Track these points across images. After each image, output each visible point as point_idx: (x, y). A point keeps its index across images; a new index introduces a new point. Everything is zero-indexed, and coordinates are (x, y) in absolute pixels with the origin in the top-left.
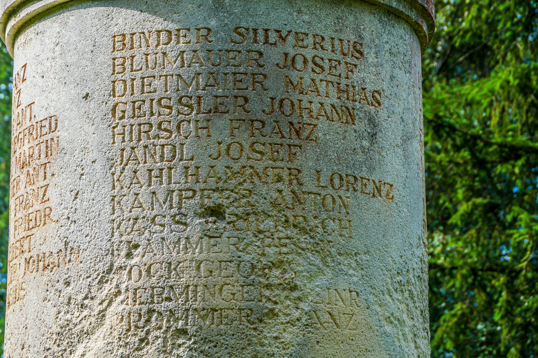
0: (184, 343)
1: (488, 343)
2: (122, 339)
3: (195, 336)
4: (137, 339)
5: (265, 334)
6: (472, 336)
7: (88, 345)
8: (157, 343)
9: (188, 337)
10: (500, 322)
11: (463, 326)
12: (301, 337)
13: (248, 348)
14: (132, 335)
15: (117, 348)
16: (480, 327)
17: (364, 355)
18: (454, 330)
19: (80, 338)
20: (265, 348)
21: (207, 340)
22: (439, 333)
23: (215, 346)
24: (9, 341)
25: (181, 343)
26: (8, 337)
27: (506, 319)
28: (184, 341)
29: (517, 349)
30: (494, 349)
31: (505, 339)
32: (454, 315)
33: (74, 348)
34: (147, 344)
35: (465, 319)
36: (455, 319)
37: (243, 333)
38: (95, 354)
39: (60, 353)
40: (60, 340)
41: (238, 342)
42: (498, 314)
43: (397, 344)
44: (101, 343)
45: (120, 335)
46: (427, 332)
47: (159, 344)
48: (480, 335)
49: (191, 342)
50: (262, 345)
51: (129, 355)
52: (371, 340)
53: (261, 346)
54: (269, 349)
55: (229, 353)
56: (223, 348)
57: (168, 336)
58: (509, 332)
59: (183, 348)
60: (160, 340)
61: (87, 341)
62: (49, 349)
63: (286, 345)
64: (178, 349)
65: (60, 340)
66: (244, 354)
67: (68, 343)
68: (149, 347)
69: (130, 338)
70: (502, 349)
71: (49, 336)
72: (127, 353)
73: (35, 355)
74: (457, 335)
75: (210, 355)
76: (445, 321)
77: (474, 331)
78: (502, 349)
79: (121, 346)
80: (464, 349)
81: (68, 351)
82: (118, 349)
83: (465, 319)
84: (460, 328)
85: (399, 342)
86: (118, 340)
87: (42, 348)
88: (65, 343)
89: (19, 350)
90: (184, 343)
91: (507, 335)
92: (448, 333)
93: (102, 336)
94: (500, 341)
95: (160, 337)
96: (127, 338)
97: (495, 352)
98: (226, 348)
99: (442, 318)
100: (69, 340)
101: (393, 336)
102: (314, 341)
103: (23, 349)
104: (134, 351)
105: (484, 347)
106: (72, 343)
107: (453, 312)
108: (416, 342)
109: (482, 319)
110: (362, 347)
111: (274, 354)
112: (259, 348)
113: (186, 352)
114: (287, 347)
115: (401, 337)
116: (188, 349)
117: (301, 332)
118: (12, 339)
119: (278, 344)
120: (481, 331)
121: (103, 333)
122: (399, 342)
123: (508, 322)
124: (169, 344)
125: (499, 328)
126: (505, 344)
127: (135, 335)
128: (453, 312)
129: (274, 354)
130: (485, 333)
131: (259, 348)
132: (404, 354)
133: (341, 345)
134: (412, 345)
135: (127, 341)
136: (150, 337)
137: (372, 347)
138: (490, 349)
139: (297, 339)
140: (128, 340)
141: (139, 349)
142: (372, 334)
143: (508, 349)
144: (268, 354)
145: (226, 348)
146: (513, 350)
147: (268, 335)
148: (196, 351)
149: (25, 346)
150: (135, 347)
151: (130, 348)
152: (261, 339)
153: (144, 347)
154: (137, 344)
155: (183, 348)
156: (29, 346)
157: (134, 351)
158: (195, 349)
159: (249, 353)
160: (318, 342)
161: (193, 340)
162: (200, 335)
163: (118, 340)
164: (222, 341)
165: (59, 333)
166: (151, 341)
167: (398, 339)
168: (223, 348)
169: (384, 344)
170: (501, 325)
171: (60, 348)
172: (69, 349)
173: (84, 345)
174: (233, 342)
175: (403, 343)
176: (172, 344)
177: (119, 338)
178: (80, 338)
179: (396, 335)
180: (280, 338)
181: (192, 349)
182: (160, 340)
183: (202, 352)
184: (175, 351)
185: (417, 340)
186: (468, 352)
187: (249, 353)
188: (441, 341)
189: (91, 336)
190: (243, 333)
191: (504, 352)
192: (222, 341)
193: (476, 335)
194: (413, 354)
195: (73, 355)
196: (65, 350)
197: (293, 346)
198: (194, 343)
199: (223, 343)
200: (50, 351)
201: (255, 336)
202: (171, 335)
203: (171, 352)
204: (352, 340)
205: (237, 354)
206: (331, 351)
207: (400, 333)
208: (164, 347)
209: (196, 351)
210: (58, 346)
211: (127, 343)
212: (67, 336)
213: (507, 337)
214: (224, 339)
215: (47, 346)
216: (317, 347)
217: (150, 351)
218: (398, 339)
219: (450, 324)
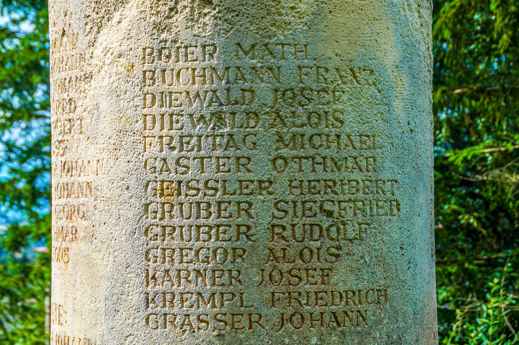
0: (209, 13)
1: (483, 31)
2: (154, 8)
3: (219, 6)
4: (167, 8)
5: (283, 4)
6: (468, 26)
7: (124, 13)
8: (185, 12)
9: (213, 6)
10: (495, 12)
11: (460, 17)
12: (315, 7)
13: (267, 17)
14: (163, 5)
15: (149, 16)
16: (476, 17)
17: (372, 23)
18: (452, 20)
19: (116, 6)
20: (282, 17)
21: (230, 10)
22: (439, 23)
23: (238, 15)
24: (53, 9)
25: (207, 12)
26: (52, 5)
27: (501, 8)
28: (209, 10)
29: (508, 36)
30: (487, 37)
31: (498, 27)
32: (453, 7)
33: (111, 16)
34: (177, 12)
35: (463, 10)
36: (454, 10)
37: (263, 4)
38: (130, 22)
39: (99, 20)
40: (98, 8)
41: (258, 11)
42: (494, 3)
43: (403, 13)
44: (135, 12)
45: (152, 4)
46: (430, 3)
47: (187, 13)
48: (476, 24)
49: (215, 12)
50: (280, 14)
51: (160, 22)
52: (379, 10)
53: (279, 15)
54: (286, 18)
55: (250, 22)
56: (245, 17)
57: (195, 6)
58: (503, 20)
59: (209, 17)
60: (188, 10)
61: (123, 9)
62: (89, 16)
63: (301, 14)
64: (204, 18)
65: (98, 8)
66: (264, 23)
67: (105, 11)
68: (178, 15)
69: (160, 7)
70: (495, 36)
71: (88, 4)
72: (159, 21)
73: (77, 22)
74: (455, 24)
75: (232, 23)
76: (444, 13)
77: (471, 21)
78: (495, 36)
79: (153, 14)
80: (460, 38)
81: (106, 19)
82: (150, 17)
83: (463, 10)
84: (458, 19)
85: (405, 11)
86: (150, 8)
87: (83, 16)
88: (103, 11)
89: (62, 17)
90: (209, 13)
91: (501, 23)
92: (446, 24)
93: (135, 5)
94: (493, 30)
95: (188, 7)
96: (158, 7)
97: (488, 40)
98: (247, 17)
99: (442, 10)
100: (106, 8)
101: (399, 6)
102: (327, 10)
103: (65, 15)
104: (165, 19)
105: (478, 36)
106: (109, 11)
107: (452, 4)
108: (419, 12)
109: (479, 9)
110: (371, 16)
111: (290, 23)
112: (277, 17)
113: (212, 21)
114: (302, 16)
115: (406, 7)
116: (213, 18)
117: (316, 3)
118: (55, 7)
119: (294, 14)
120: (478, 21)
121: (136, 2)
122: (405, 11)
123: (502, 11)
124: (195, 13)
125: (493, 17)
126: (498, 31)
127: (165, 4)
128: (452, 4)
129: (290, 23)
130: (481, 22)
131: (277, 17)
132: (408, 22)
133: (351, 14)
134: (416, 14)
135: (158, 10)
136: (179, 7)
137: (380, 16)
138: (484, 37)
139: (312, 9)
140: (159, 9)
141: (169, 17)
142: (380, 4)
143: (500, 36)
144: (285, 23)
145: (247, 17)
146: (505, 37)
147: (285, 5)
148: (220, 20)
149: (67, 13)
150: (166, 15)
151: (161, 17)
152: (279, 9)
153: (173, 16)
154: (167, 13)
155: (209, 17)
156: (71, 14)
157: (165, 19)
158: (220, 18)
159: (268, 22)
160: (330, 12)
161: (217, 10)
162: (224, 5)
163: (150, 8)
164: (244, 11)
165: (97, 2)
166: (179, 10)
167: (404, 9)
168: (245, 17)
169: (390, 13)
170: (496, 15)
171: (99, 16)
172: (107, 17)
173: (119, 13)
174: (253, 11)
175: (408, 13)
176: (199, 13)
177: (151, 7)
178: (116, 6)
179: (402, 5)
180: (296, 8)
181: (217, 18)
182: (188, 10)
183: (225, 20)
184: (201, 20)
185: (421, 10)
186: (463, 40)
187: (268, 22)
188: (440, 30)
189: (126, 5)
190: (263, 4)
191: (496, 39)
192: (244, 11)
193: (472, 24)
194: (416, 23)
195: (110, 22)
196: (103, 17)
197: (308, 15)
198: (219, 12)
199: (244, 13)
200: (90, 18)
201: (273, 7)
202: (198, 5)
203: (198, 20)
204: (362, 9)
205: (257, 23)
206: (342, 20)
207: (406, 4)
208: (191, 15)
209: (220, 20)
210: (97, 13)
211: (158, 12)
212: (104, 5)
213: (500, 25)
214: (245, 9)
215: (87, 13)
216: (330, 16)
217: (179, 19)
218: (404, 9)
219: (449, 15)
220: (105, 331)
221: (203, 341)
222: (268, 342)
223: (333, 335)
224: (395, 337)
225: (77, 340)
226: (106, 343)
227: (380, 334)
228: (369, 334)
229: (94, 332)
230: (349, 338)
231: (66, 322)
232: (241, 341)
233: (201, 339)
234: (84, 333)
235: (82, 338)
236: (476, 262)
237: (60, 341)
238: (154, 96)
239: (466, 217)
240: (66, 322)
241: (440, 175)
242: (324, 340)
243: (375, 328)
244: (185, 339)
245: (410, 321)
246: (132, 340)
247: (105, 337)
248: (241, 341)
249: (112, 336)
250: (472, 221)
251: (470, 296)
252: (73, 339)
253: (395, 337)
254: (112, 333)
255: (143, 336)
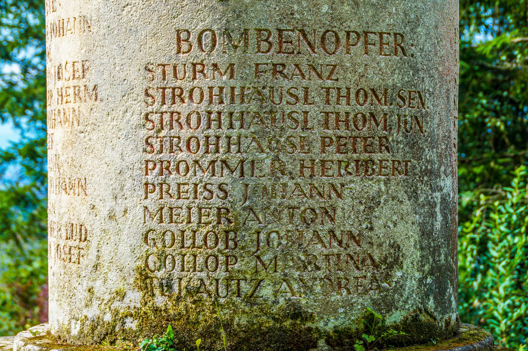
220: (100, 4)
221: (205, 6)
222: (276, 8)
223: (346, 5)
224: (412, 16)
225: (72, 20)
226: (102, 16)
227: (396, 10)
228: (385, 8)
229: (90, 6)
230: (363, 10)
231: (60, 5)
232: (246, 6)
233: (203, 5)
234: (79, 10)
235: (77, 16)
236: (501, 161)
237: (55, 28)
238: (183, 91)
239: (493, 120)
240: (60, 5)
241: (467, 66)
242: (335, 9)
243: (391, 3)
244: (186, 5)
245: (429, 3)
246: (130, 10)
247: (101, 11)
248: (246, 6)
249: (108, 8)
250: (498, 124)
251: (495, 186)
252: (67, 20)
253: (412, 16)
254: (108, 5)
255: (141, 5)
